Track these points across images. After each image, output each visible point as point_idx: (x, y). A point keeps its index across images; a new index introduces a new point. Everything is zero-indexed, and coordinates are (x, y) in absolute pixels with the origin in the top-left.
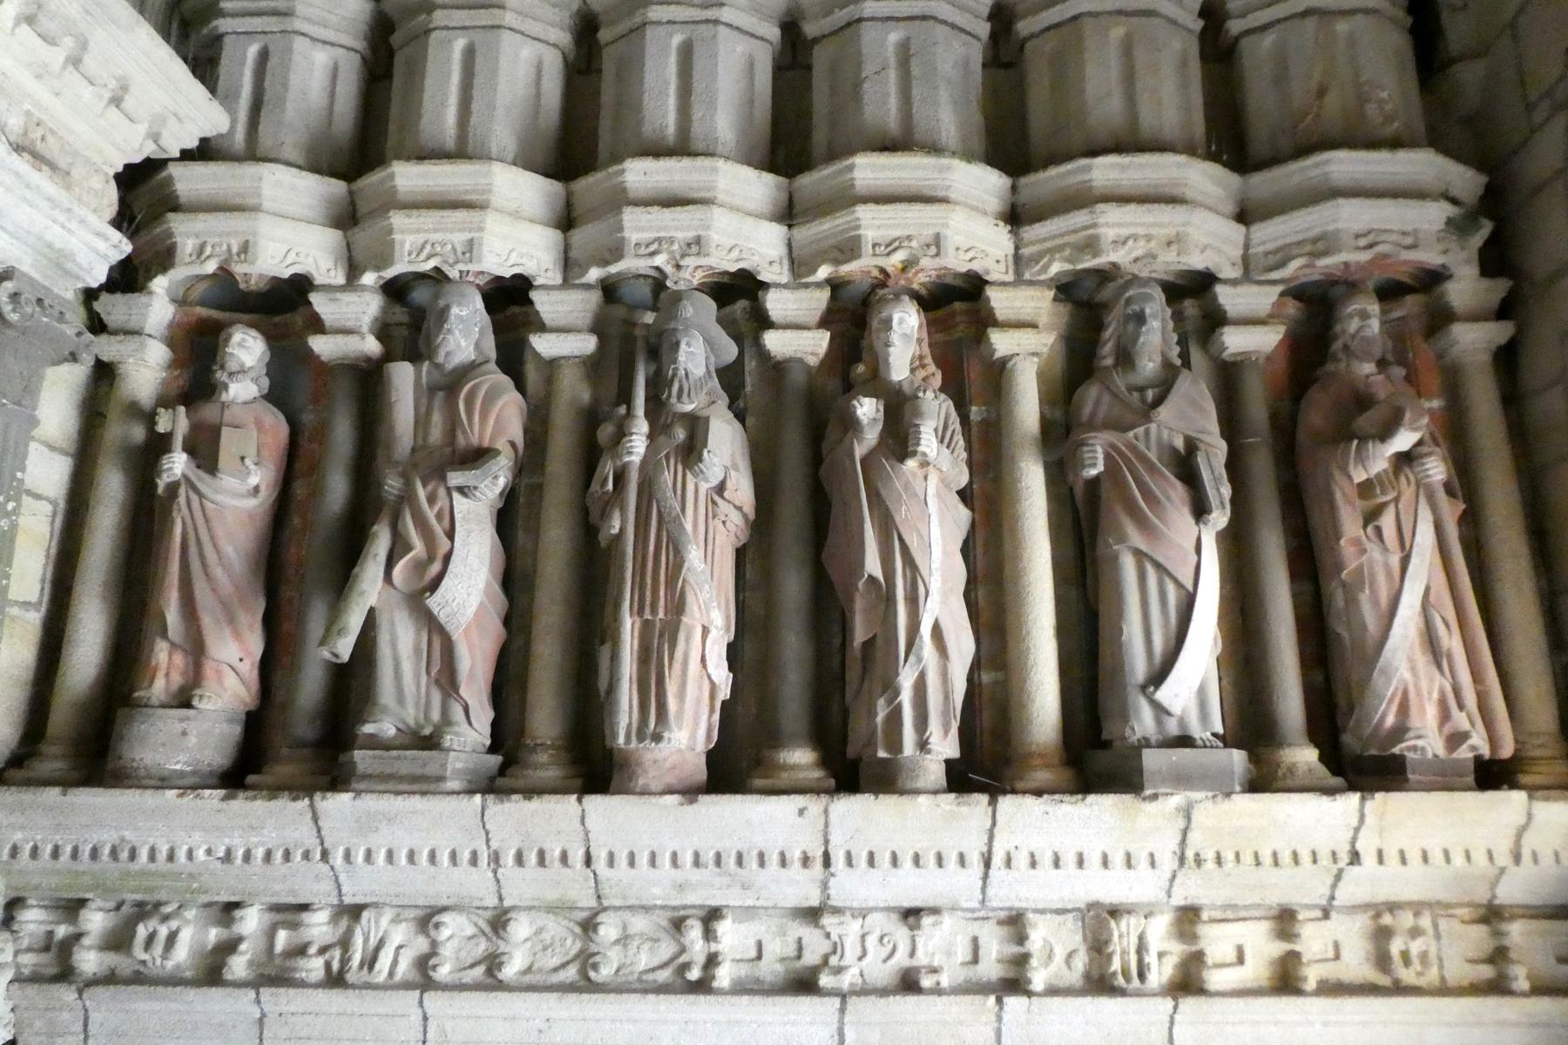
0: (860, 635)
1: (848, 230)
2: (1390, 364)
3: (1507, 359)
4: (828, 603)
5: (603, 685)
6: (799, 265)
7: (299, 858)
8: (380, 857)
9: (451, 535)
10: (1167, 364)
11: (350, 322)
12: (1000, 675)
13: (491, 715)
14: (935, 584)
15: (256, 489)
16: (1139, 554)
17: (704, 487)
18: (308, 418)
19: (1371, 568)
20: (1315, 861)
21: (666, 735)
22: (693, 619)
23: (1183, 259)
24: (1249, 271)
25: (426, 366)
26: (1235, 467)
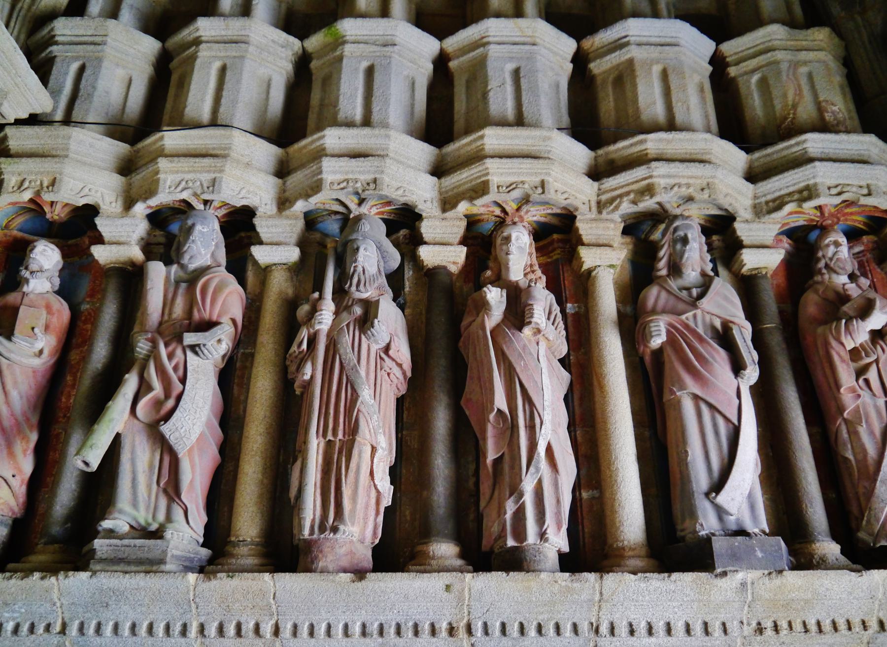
0: (491, 455)
1: (480, 177)
2: (858, 277)
4: (465, 439)
6: (447, 203)
7: (41, 631)
8: (108, 630)
9: (183, 381)
10: (703, 274)
12: (596, 493)
13: (205, 519)
14: (547, 417)
15: (41, 352)
16: (696, 398)
17: (375, 348)
19: (865, 409)
20: (850, 629)
21: (342, 527)
25: (174, 268)
26: (758, 340)
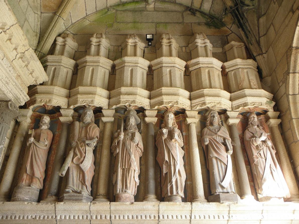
0: (164, 172)
1: (161, 100)
3: (281, 126)
4: (158, 167)
5: (114, 182)
6: (152, 106)
9: (85, 153)
11: (67, 115)
14: (178, 163)
15: (46, 145)
18: (57, 133)
19: (259, 161)
22: (132, 168)
23: (221, 106)
24: (233, 109)
